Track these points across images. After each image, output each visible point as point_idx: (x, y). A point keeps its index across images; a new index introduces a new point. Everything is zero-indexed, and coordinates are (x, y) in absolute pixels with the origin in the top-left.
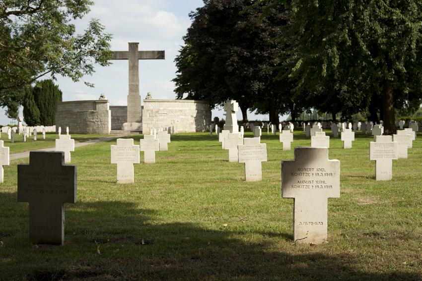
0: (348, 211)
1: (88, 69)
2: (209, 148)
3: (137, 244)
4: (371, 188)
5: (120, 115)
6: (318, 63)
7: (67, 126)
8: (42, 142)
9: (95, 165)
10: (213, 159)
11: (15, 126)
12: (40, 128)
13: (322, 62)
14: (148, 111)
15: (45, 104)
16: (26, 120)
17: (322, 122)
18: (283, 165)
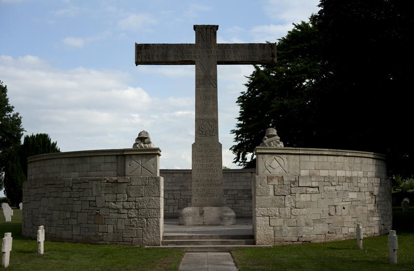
14: (270, 178)
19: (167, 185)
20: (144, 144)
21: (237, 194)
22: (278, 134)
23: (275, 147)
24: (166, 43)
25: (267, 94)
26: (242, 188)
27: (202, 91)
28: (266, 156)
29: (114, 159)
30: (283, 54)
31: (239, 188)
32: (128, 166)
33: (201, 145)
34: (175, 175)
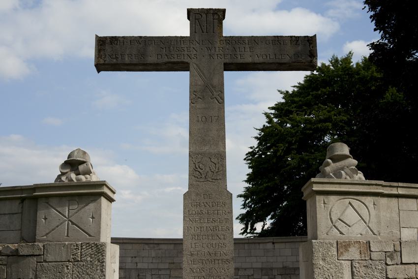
5: (145, 266)
14: (342, 247)
19: (151, 261)
20: (77, 174)
21: (253, 275)
22: (354, 153)
23: (349, 180)
24: (143, 35)
25: (281, 147)
26: (259, 265)
27: (200, 85)
28: (333, 198)
29: (15, 207)
30: (300, 101)
31: (255, 266)
32: (41, 221)
33: (197, 194)
34: (162, 247)
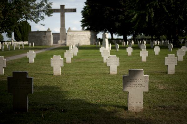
0: (153, 93)
1: (42, 18)
2: (95, 54)
3: (60, 111)
4: (165, 79)
6: (145, 15)
7: (33, 42)
8: (23, 50)
9: (44, 64)
10: (97, 61)
11: (11, 41)
12: (21, 43)
13: (146, 15)
14: (69, 35)
15: (23, 32)
16: (15, 38)
17: (147, 40)
18: (123, 77)
